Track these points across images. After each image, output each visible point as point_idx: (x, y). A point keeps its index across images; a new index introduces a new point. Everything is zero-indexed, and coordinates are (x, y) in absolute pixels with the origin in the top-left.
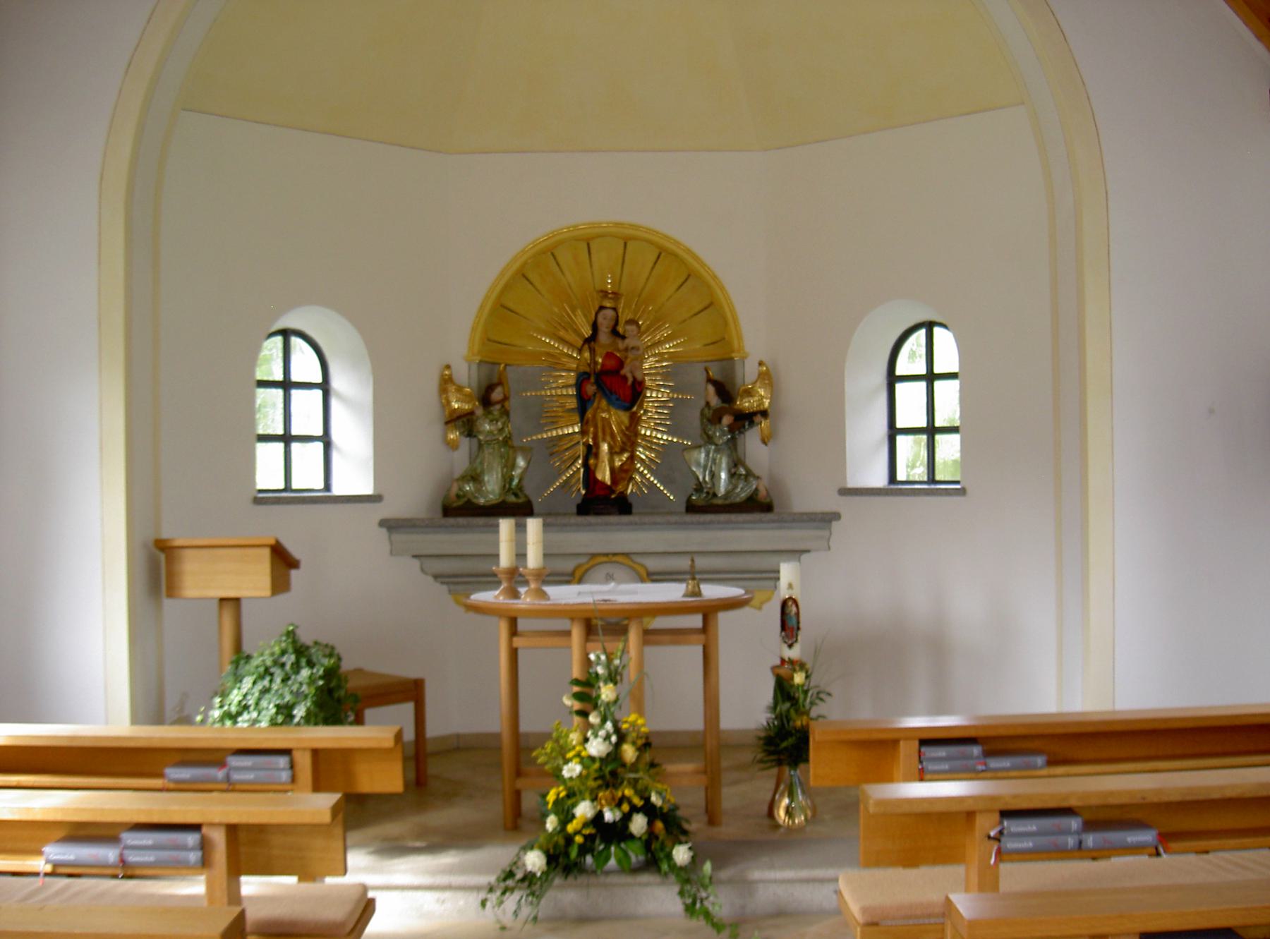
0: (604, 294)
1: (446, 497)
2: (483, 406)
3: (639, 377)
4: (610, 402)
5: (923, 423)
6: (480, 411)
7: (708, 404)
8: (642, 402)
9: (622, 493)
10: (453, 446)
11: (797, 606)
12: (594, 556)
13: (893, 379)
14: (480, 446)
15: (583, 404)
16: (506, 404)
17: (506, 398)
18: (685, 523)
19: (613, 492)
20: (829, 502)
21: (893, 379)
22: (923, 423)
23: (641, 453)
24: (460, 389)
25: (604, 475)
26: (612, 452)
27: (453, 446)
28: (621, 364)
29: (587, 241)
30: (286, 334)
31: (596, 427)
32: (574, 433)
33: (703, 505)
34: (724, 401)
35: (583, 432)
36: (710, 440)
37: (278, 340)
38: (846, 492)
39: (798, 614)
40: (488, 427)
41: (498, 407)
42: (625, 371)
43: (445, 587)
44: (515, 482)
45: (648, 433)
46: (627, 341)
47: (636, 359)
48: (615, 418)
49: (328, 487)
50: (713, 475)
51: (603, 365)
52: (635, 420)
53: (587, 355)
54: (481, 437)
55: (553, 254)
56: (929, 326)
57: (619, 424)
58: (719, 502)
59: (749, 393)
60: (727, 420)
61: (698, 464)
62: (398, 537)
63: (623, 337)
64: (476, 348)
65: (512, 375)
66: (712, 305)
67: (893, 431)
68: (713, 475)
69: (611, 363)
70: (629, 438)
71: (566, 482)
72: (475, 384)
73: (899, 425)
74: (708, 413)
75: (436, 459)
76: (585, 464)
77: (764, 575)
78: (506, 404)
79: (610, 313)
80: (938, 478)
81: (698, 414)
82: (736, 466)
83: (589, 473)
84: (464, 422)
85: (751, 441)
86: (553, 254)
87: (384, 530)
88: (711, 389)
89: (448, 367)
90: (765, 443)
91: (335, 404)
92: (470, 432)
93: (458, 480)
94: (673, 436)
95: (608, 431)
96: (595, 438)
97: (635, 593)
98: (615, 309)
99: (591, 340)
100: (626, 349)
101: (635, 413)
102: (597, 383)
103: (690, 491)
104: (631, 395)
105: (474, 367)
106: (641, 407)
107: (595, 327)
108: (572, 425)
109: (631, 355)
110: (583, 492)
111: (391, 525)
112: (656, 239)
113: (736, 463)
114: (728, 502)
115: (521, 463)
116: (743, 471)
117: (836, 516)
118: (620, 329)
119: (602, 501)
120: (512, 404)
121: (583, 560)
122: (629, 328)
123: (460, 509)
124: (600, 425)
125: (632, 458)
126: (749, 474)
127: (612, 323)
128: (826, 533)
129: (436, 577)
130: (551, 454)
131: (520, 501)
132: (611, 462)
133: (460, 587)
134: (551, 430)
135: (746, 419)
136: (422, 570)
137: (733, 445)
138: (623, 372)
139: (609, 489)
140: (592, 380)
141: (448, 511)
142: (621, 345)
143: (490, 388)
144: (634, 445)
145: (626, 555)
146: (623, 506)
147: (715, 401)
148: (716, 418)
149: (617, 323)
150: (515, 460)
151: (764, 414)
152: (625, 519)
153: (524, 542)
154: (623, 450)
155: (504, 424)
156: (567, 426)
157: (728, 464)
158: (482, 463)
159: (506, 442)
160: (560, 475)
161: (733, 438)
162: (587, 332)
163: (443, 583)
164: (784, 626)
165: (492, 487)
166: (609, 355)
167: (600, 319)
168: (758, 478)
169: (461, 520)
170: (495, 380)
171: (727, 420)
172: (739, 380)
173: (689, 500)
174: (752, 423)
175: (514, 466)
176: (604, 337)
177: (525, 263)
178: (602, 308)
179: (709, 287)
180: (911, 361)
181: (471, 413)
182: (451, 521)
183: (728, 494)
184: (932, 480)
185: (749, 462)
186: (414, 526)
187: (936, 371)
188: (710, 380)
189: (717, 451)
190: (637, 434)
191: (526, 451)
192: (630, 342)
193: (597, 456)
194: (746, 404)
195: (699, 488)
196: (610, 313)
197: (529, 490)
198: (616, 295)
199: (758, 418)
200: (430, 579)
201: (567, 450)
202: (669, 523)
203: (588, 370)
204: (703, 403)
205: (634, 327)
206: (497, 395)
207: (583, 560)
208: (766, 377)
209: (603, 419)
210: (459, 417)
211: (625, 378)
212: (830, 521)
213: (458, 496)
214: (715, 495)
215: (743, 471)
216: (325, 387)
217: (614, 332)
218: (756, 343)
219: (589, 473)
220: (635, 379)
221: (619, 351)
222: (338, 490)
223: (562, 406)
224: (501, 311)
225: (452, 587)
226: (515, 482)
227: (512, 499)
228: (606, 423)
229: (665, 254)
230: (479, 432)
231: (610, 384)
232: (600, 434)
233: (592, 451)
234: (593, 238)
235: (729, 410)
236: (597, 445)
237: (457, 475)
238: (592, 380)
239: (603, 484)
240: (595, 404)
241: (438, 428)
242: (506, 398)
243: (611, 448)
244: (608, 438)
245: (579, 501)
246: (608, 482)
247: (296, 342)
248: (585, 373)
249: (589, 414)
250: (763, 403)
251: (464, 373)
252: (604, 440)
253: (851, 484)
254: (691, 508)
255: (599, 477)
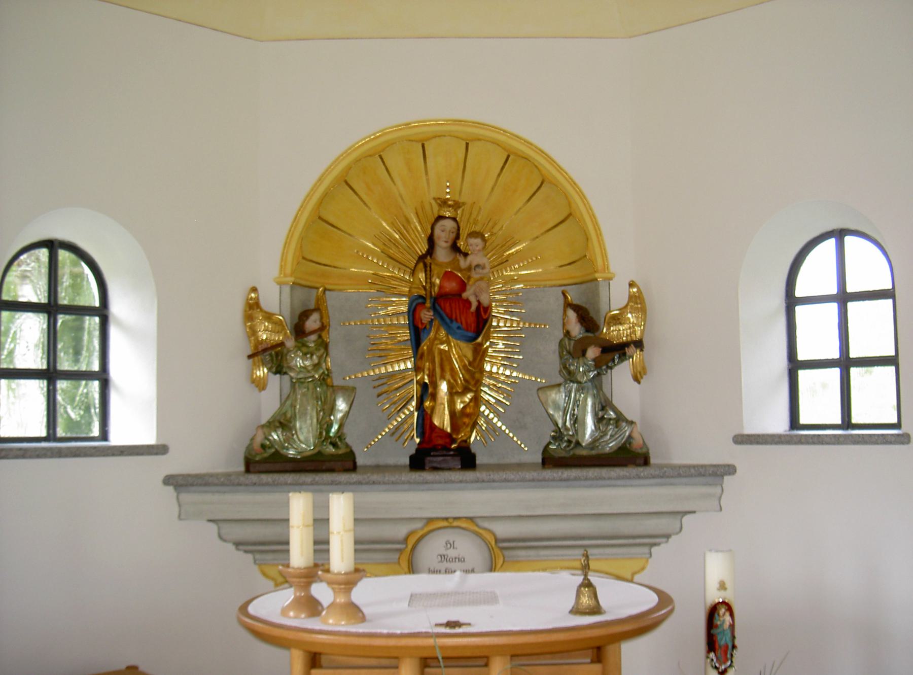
0: (444, 203)
1: (249, 448)
2: (294, 339)
3: (485, 302)
4: (450, 331)
5: (834, 353)
6: (290, 343)
7: (567, 334)
8: (488, 332)
9: (465, 441)
10: (261, 385)
11: (732, 615)
12: (430, 520)
13: (792, 301)
14: (293, 385)
15: (417, 333)
16: (324, 334)
17: (323, 328)
18: (544, 480)
19: (454, 441)
20: (717, 451)
21: (792, 301)
22: (834, 353)
23: (488, 395)
24: (269, 317)
25: (443, 420)
26: (452, 393)
27: (261, 385)
28: (463, 286)
29: (422, 144)
30: (52, 245)
31: (433, 362)
32: (407, 370)
33: (564, 457)
34: (587, 331)
35: (417, 369)
36: (570, 376)
37: (43, 254)
38: (742, 439)
39: (732, 626)
40: (299, 362)
41: (313, 337)
42: (468, 294)
43: (250, 557)
44: (335, 427)
45: (495, 370)
46: (469, 258)
47: (481, 279)
48: (457, 351)
49: (104, 436)
50: (577, 421)
51: (441, 287)
52: (480, 354)
53: (422, 276)
54: (292, 374)
55: (381, 157)
56: (840, 234)
57: (460, 358)
58: (584, 453)
59: (617, 320)
60: (593, 352)
61: (557, 407)
62: (186, 497)
63: (466, 255)
64: (289, 270)
65: (332, 300)
66: (570, 216)
67: (795, 365)
68: (575, 420)
69: (451, 286)
70: (472, 375)
71: (397, 428)
72: (287, 313)
73: (802, 356)
74: (569, 345)
75: (242, 402)
76: (420, 407)
77: (638, 541)
78: (324, 334)
79: (449, 224)
80: (803, 420)
81: (554, 346)
82: (603, 408)
83: (425, 418)
84: (272, 356)
85: (620, 377)
86: (381, 157)
87: (171, 488)
88: (572, 315)
89: (254, 290)
90: (637, 379)
91: (114, 333)
92: (279, 369)
93: (263, 426)
94: (525, 374)
95: (447, 368)
96: (432, 376)
97: (491, 599)
98: (454, 219)
99: (426, 259)
100: (469, 269)
101: (481, 345)
102: (434, 308)
103: (547, 439)
104: (478, 323)
105: (287, 290)
106: (487, 338)
107: (431, 241)
108: (404, 360)
109: (475, 275)
110: (418, 440)
111: (179, 483)
112: (502, 138)
113: (603, 405)
114: (594, 452)
115: (342, 405)
116: (612, 414)
117: (730, 470)
118: (461, 244)
119: (441, 451)
120: (333, 336)
121: (419, 525)
122: (473, 241)
123: (267, 463)
124: (437, 360)
125: (477, 400)
126: (620, 419)
127: (453, 236)
128: (718, 490)
129: (238, 544)
130: (379, 396)
131: (340, 452)
132: (452, 403)
133: (269, 557)
134: (378, 366)
135: (616, 351)
136: (220, 537)
137: (597, 383)
138: (465, 295)
139: (450, 438)
140: (428, 304)
141: (251, 465)
142: (463, 263)
143: (305, 315)
144: (478, 383)
145: (471, 519)
146: (467, 459)
147: (576, 330)
148: (580, 351)
149: (458, 237)
150: (335, 401)
151: (639, 344)
152: (469, 475)
153: (325, 520)
154: (466, 390)
155: (320, 358)
156: (398, 362)
157: (594, 405)
158: (293, 406)
159: (325, 379)
160: (390, 418)
161: (599, 374)
162: (423, 248)
163: (246, 552)
164: (711, 644)
165: (304, 439)
166: (448, 276)
167: (437, 231)
168: (631, 423)
169: (265, 478)
170: (312, 307)
171: (593, 352)
172: (604, 308)
173: (546, 449)
174: (623, 357)
175: (332, 409)
176: (442, 254)
177: (349, 168)
178: (440, 218)
179: (566, 196)
180: (817, 274)
181: (282, 344)
182: (253, 478)
183: (595, 441)
184: (847, 422)
185: (615, 402)
186: (207, 484)
187: (850, 289)
188: (568, 305)
189: (581, 388)
190: (482, 370)
191: (349, 392)
192: (473, 259)
193: (434, 397)
194: (618, 333)
195: (558, 436)
196: (449, 224)
197: (351, 439)
198: (457, 205)
199: (630, 350)
200: (231, 547)
201: (397, 389)
202: (523, 480)
203: (423, 293)
204: (560, 334)
205: (478, 241)
206: (312, 323)
207: (419, 525)
208: (637, 301)
209: (442, 351)
210: (265, 350)
211: (468, 303)
212: (722, 476)
213: (263, 446)
214: (578, 444)
215: (612, 414)
216: (103, 312)
217: (455, 248)
218: (623, 266)
219: (425, 418)
220: (479, 302)
221: (461, 270)
222: (117, 438)
223: (393, 337)
224: (320, 222)
225: (258, 556)
226: (335, 427)
227: (332, 450)
228: (445, 357)
229: (512, 156)
230: (291, 368)
231: (450, 310)
232: (438, 370)
233: (427, 391)
234: (428, 139)
235: (595, 343)
236: (435, 386)
237: (264, 421)
238: (428, 304)
239: (442, 431)
240: (432, 334)
241: (243, 363)
242: (323, 328)
243: (451, 387)
244: (448, 376)
245: (413, 451)
246: (449, 430)
247: (64, 255)
248: (420, 297)
249: (424, 347)
250: (634, 332)
251: (273, 299)
252: (443, 377)
253: (748, 430)
254: (549, 461)
255: (436, 422)
